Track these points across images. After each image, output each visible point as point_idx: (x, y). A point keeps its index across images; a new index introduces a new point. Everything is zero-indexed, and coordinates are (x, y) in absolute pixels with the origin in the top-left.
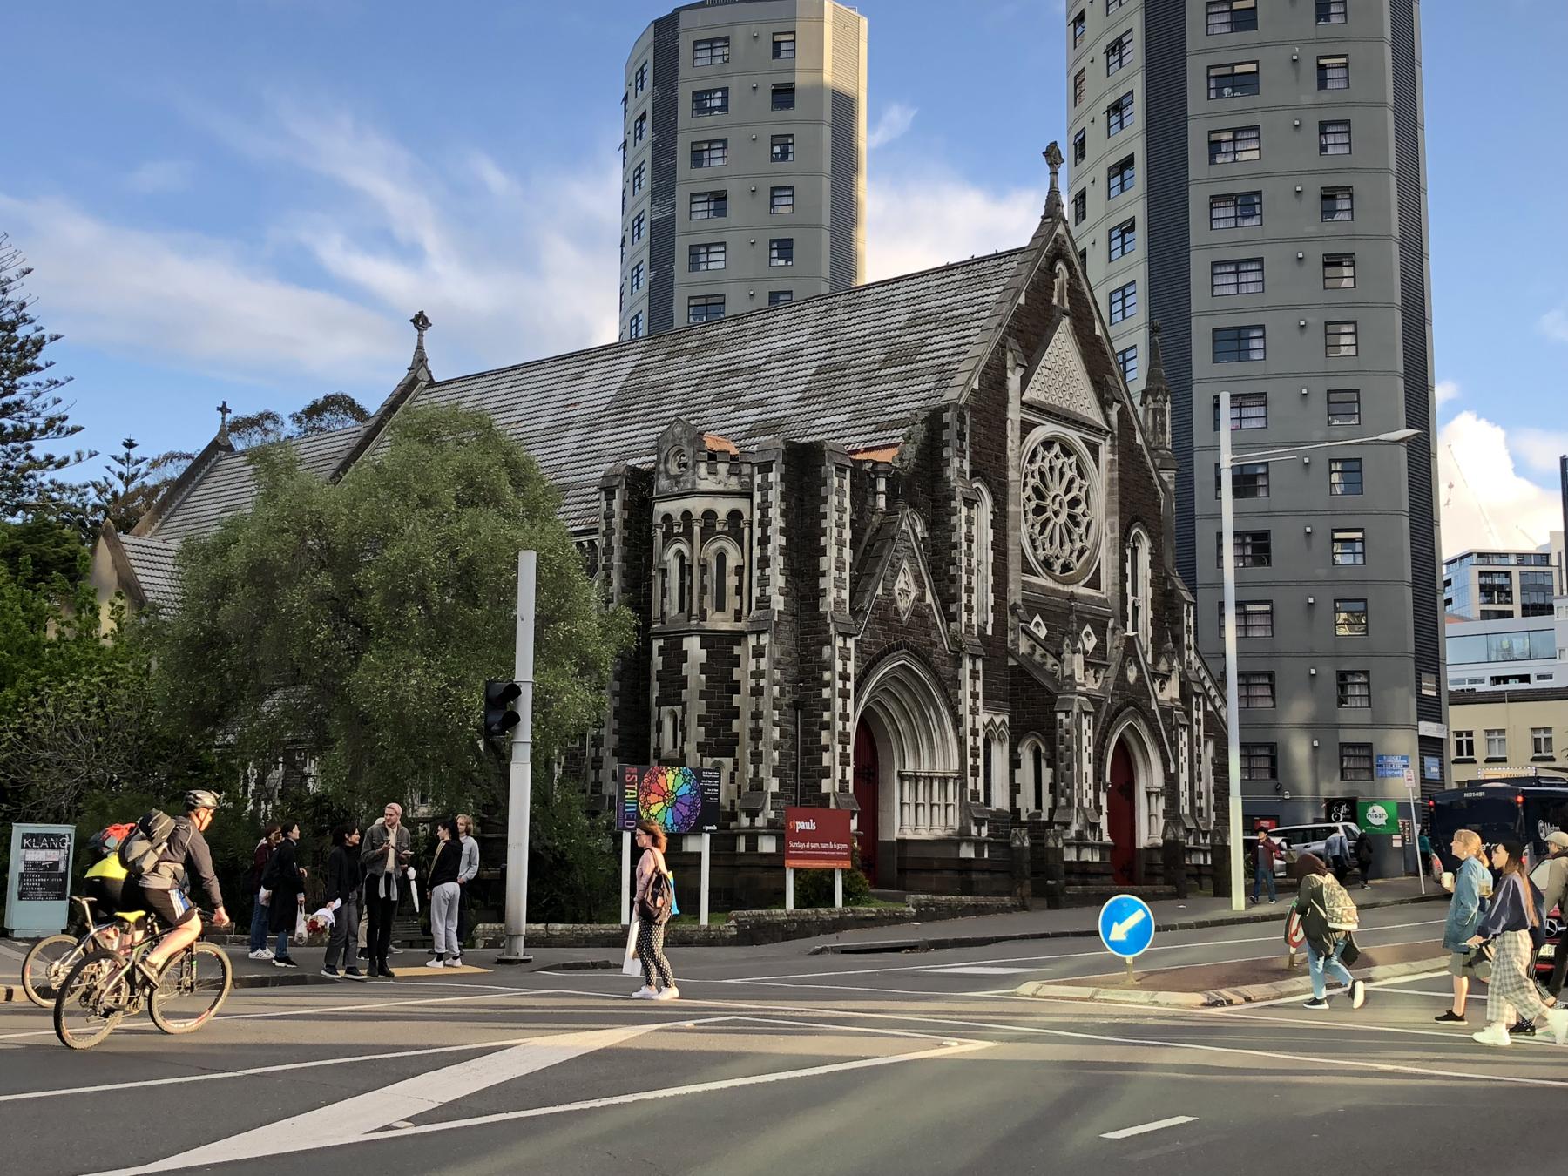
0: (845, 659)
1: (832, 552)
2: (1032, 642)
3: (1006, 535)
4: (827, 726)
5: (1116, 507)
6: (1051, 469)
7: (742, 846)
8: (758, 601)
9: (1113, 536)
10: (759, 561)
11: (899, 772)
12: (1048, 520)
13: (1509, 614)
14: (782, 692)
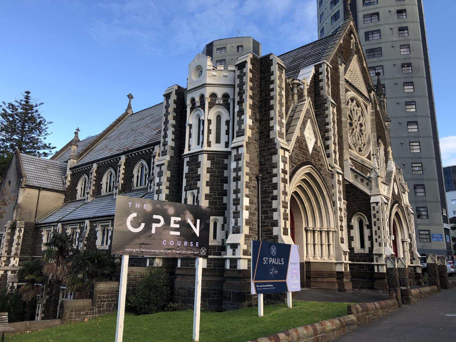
0: (285, 162)
1: (277, 107)
2: (355, 174)
3: (342, 130)
4: (275, 198)
5: (375, 129)
6: (354, 110)
7: (228, 266)
8: (237, 133)
9: (374, 140)
10: (238, 112)
11: (305, 228)
12: (353, 129)
13: (63, 297)
14: (250, 179)
